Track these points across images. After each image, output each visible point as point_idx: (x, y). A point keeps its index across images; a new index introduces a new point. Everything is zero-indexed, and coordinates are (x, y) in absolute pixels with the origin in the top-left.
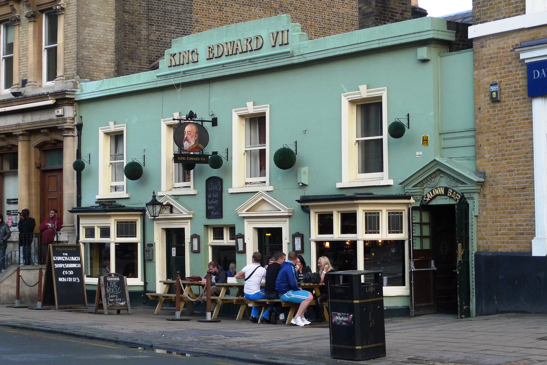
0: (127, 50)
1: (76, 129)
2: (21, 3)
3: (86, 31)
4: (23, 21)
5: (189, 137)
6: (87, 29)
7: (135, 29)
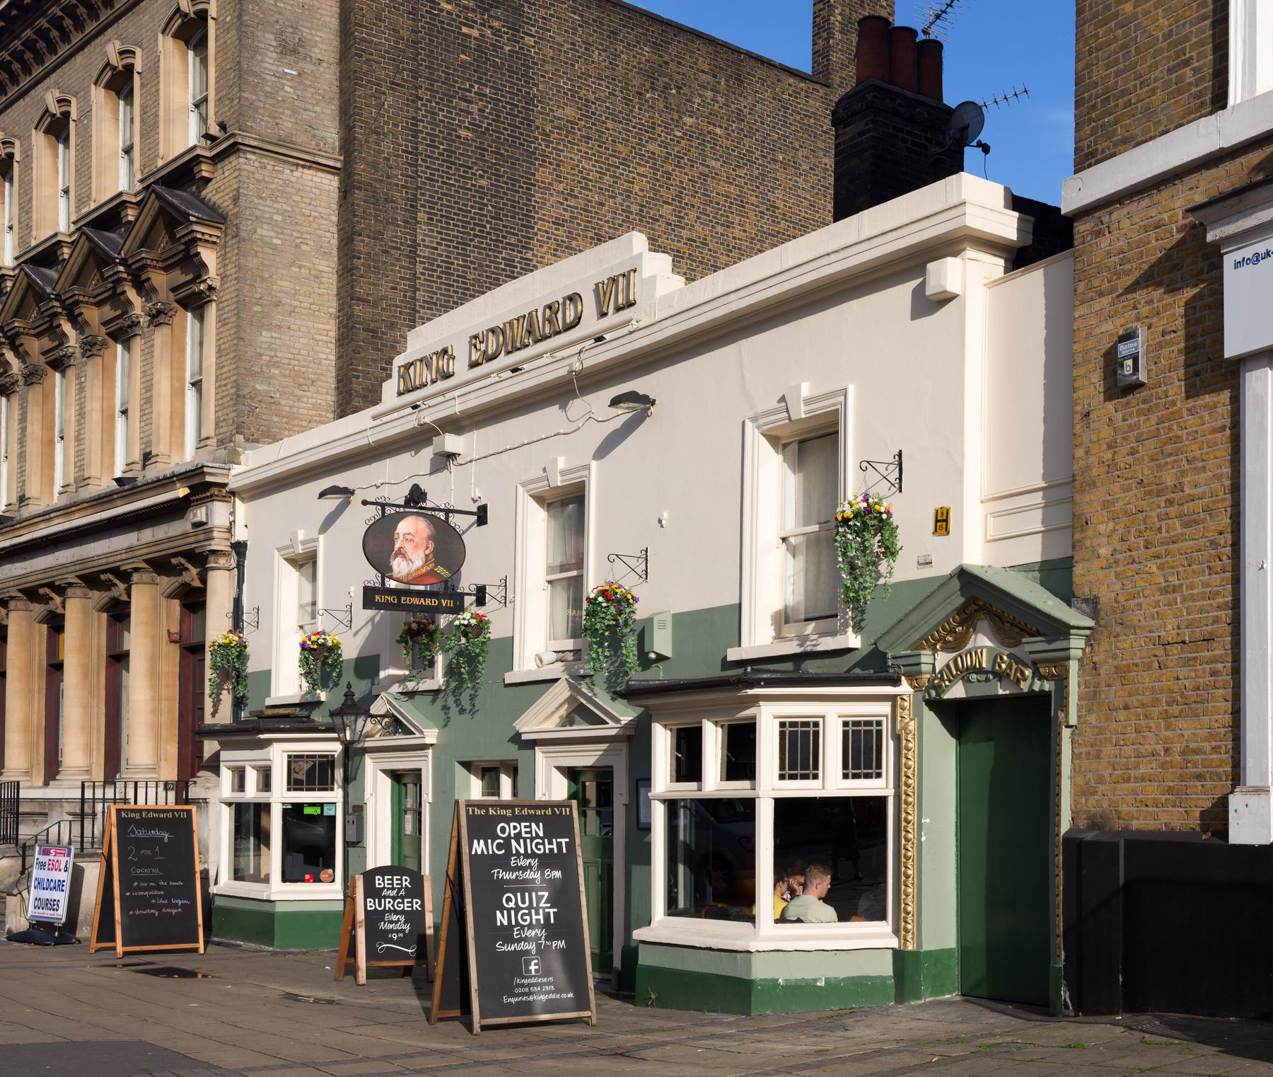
0: (359, 384)
3: (262, 339)
5: (408, 548)
6: (264, 333)
7: (381, 339)
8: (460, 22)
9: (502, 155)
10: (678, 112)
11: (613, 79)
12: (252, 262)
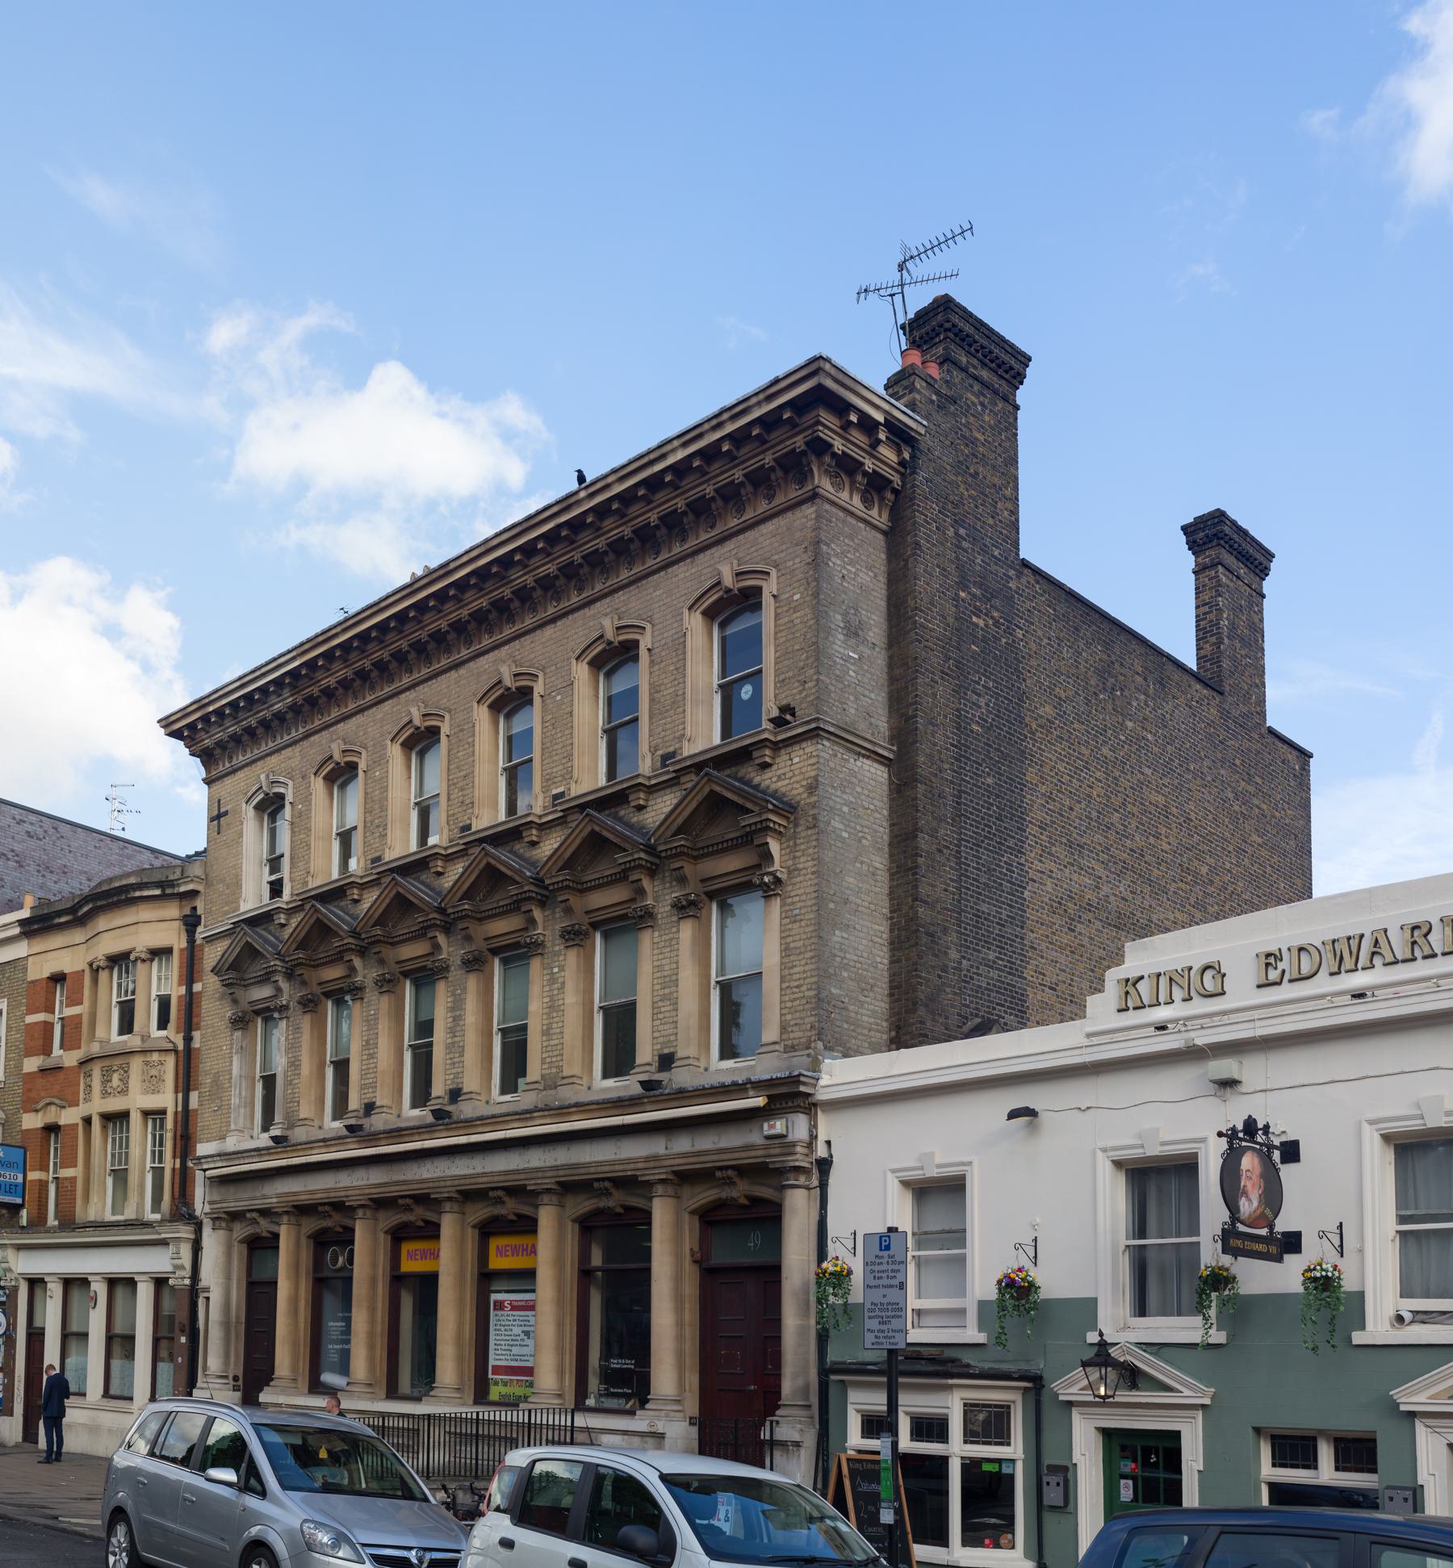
1: (815, 1171)
2: (656, 877)
3: (835, 939)
4: (662, 918)
5: (1249, 1188)
6: (837, 932)
7: (937, 944)
8: (971, 611)
9: (1002, 752)
10: (1122, 715)
11: (1078, 678)
12: (828, 856)
